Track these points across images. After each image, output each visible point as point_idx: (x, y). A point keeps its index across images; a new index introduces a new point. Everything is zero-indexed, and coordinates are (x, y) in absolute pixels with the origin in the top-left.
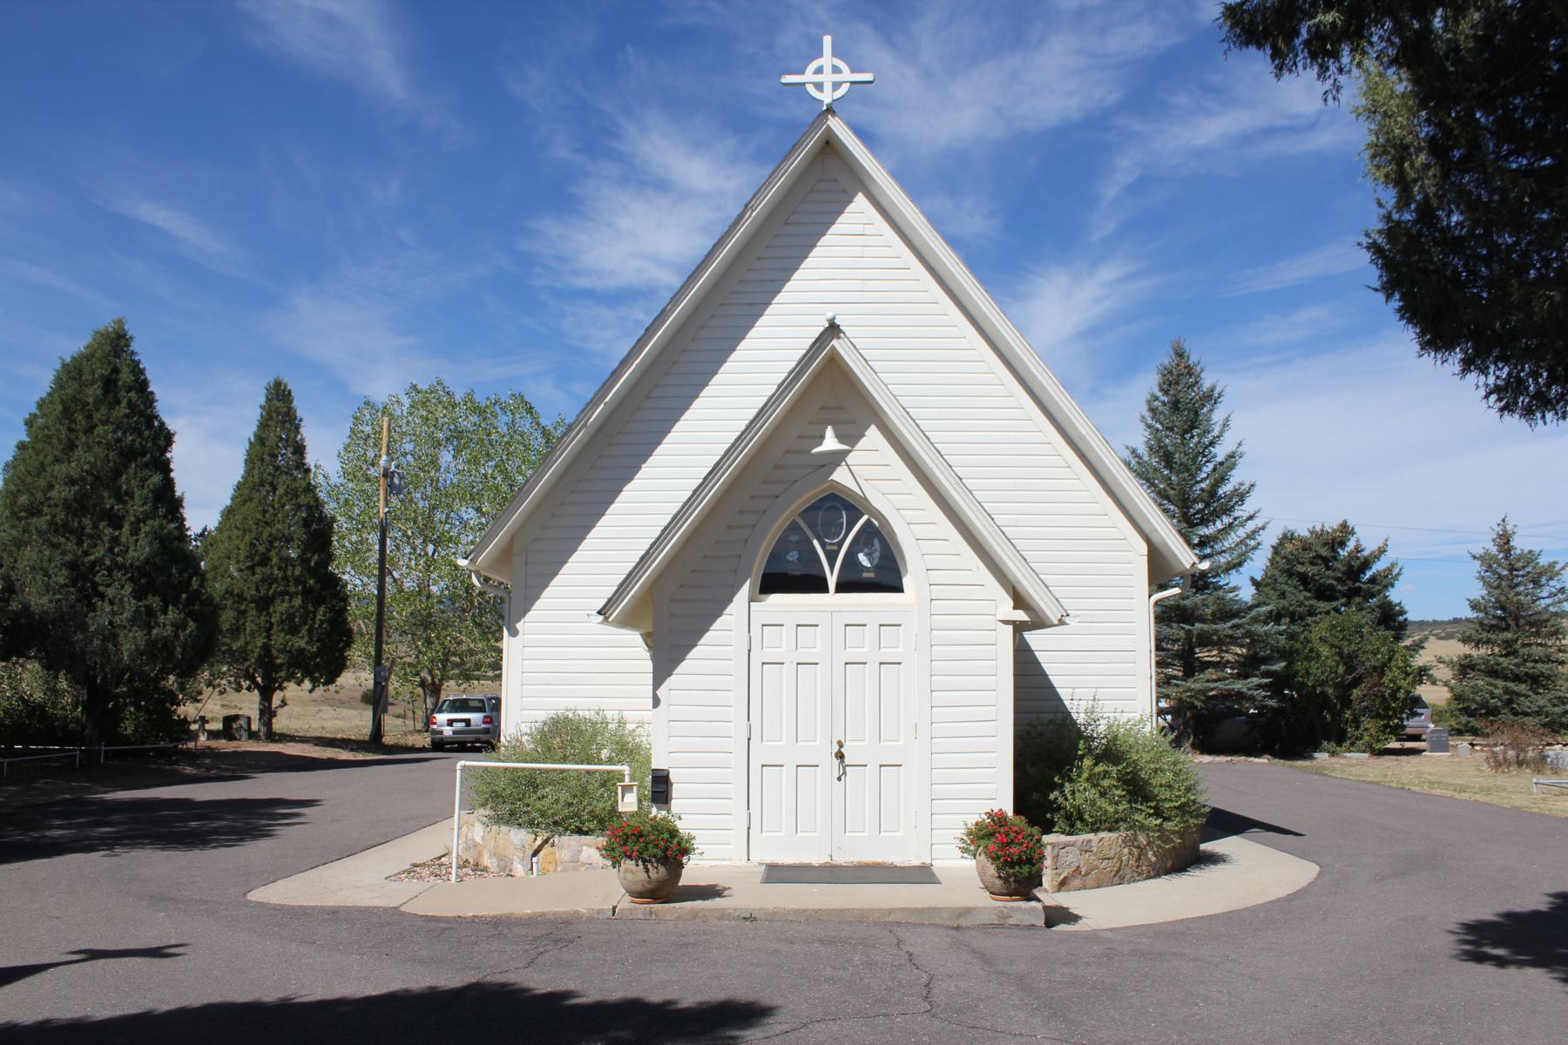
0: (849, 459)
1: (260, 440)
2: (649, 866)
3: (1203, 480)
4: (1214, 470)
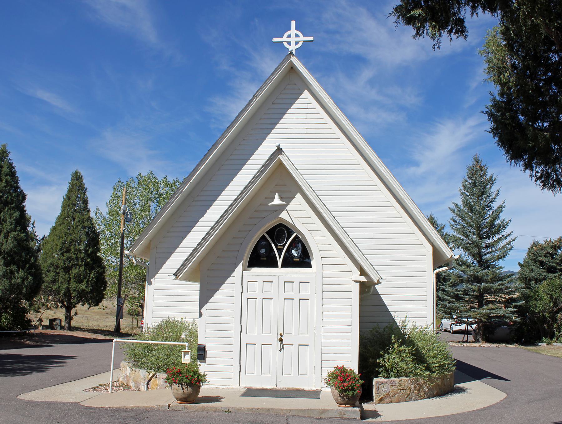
0: (288, 208)
1: (68, 197)
2: (184, 387)
3: (488, 218)
4: (492, 213)
